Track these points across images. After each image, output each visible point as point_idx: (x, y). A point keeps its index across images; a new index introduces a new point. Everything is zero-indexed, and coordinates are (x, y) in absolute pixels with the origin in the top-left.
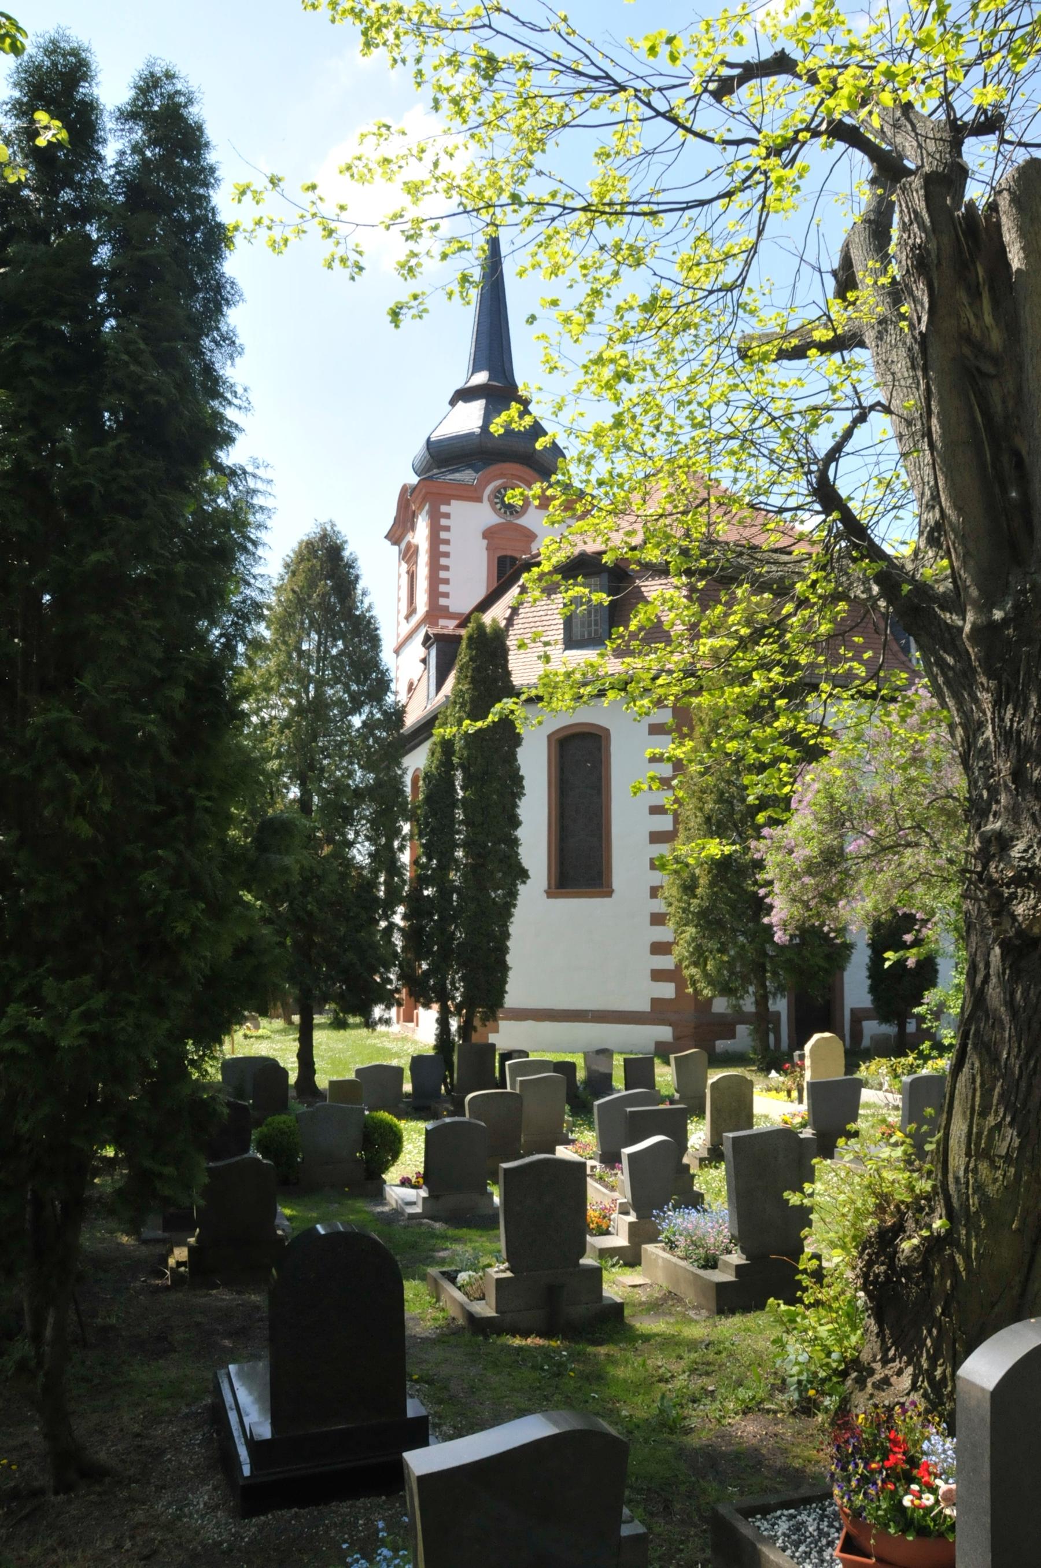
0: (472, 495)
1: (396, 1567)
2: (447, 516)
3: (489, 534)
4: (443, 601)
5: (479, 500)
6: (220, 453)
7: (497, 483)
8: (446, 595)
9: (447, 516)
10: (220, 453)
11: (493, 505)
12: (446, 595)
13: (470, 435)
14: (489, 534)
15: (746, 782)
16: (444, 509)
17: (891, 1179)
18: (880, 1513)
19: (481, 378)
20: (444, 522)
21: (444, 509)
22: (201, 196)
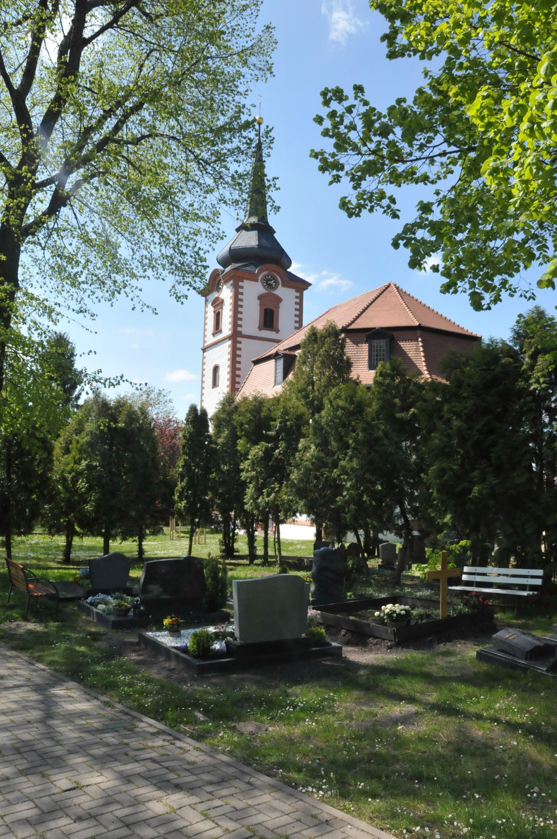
0: (254, 278)
1: (556, 39)
2: (242, 287)
3: (260, 298)
4: (239, 329)
5: (257, 281)
6: (112, 403)
7: (265, 273)
8: (241, 326)
9: (242, 287)
10: (112, 403)
11: (263, 283)
12: (241, 326)
13: (252, 249)
14: (260, 298)
15: (514, 116)
16: (241, 284)
17: (548, 156)
18: (534, 185)
19: (254, 220)
20: (240, 290)
21: (241, 284)
22: (338, 632)
